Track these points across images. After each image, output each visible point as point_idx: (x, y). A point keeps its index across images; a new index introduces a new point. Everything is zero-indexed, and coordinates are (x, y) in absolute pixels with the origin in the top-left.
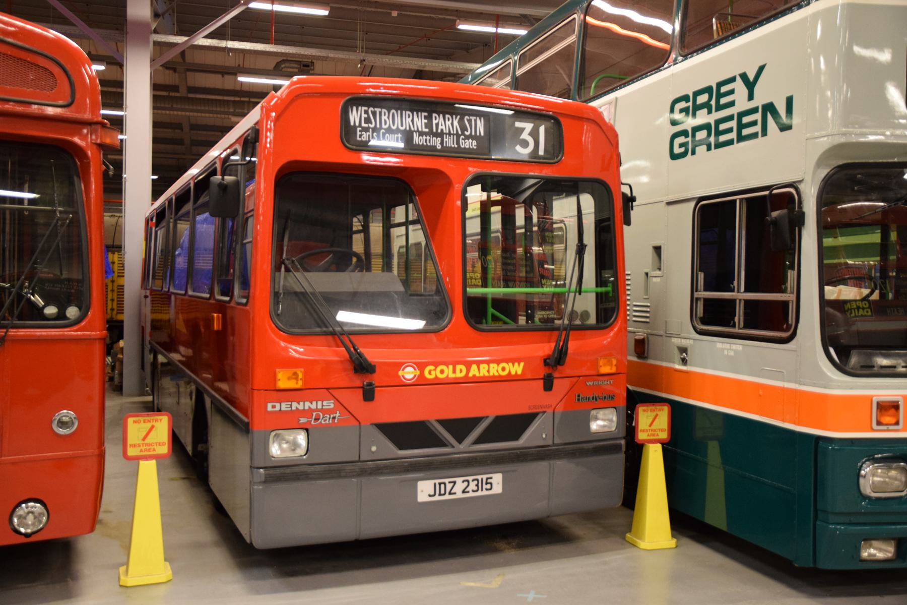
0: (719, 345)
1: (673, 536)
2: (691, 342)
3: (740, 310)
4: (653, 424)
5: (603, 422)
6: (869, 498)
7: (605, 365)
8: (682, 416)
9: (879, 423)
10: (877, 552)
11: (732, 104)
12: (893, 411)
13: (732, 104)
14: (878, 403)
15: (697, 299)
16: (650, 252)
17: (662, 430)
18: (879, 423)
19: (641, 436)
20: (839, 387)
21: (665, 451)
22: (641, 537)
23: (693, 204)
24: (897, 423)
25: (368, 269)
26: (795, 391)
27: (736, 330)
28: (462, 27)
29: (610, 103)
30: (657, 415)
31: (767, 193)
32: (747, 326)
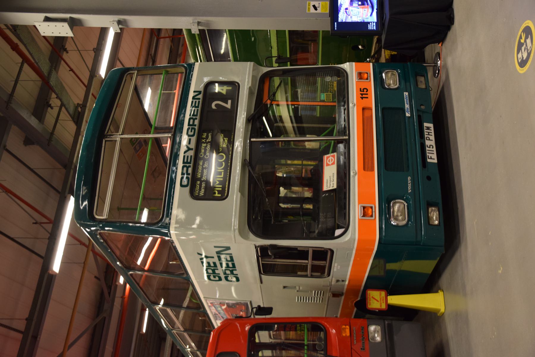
0: (335, 270)
1: (437, 292)
2: (333, 279)
3: (317, 263)
4: (377, 300)
5: (375, 332)
6: (408, 221)
7: (345, 332)
8: (374, 282)
9: (372, 216)
10: (435, 216)
11: (214, 263)
12: (365, 209)
13: (214, 263)
14: (363, 216)
15: (311, 275)
16: (285, 290)
17: (380, 294)
18: (372, 216)
19: (384, 307)
20: (355, 235)
21: (391, 295)
22: (439, 310)
23: (263, 276)
24: (372, 208)
25: (278, 32)
26: (356, 251)
27: (327, 265)
28: (144, 330)
29: (206, 300)
30: (373, 297)
31: (260, 258)
32: (325, 260)
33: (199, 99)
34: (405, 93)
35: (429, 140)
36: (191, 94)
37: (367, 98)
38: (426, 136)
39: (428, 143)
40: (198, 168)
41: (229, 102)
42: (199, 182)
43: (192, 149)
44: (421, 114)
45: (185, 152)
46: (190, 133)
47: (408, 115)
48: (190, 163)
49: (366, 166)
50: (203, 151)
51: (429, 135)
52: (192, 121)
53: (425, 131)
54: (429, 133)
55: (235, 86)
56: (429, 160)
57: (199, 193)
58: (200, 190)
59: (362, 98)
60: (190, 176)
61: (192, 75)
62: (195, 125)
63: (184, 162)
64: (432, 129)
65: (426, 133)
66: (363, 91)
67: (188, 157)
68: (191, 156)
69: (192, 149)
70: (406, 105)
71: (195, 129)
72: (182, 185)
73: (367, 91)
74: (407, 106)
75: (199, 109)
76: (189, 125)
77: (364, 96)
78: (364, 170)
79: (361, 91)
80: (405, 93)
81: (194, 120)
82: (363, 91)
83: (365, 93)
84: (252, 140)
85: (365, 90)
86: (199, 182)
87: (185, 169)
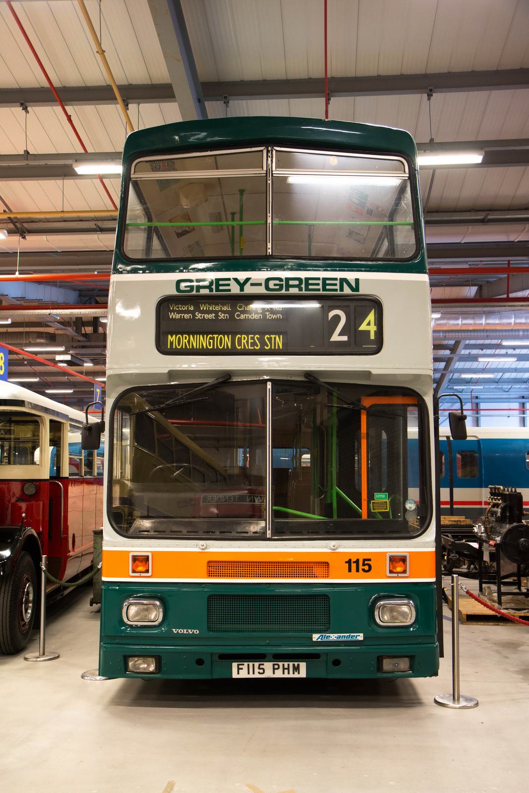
6: (131, 626)
9: (134, 571)
18: (134, 571)
33: (342, 289)
34: (362, 635)
35: (274, 669)
36: (351, 276)
37: (350, 570)
38: (281, 664)
39: (268, 666)
40: (216, 304)
41: (345, 338)
42: (192, 308)
43: (242, 289)
44: (323, 658)
45: (236, 280)
46: (271, 284)
47: (316, 637)
48: (217, 290)
49: (215, 566)
50: (486, 309)
51: (284, 669)
52: (297, 283)
53: (291, 664)
54: (288, 669)
55: (377, 346)
56: (235, 665)
57: (174, 311)
58: (179, 312)
59: (349, 562)
60: (194, 292)
61: (320, 270)
62: (287, 289)
63: (307, 279)
64: (296, 675)
65: (286, 664)
66: (364, 565)
67: (229, 285)
68: (230, 290)
69: (242, 289)
70: (336, 635)
71: (281, 289)
72: (179, 282)
73: (364, 570)
74: (333, 637)
75: (321, 292)
76: (288, 280)
77: (354, 566)
78: (209, 562)
79: (364, 560)
80: (362, 635)
81: (299, 286)
82: (364, 565)
83: (361, 567)
84: (269, 386)
85: (366, 568)
86: (192, 308)
87: (297, 283)
